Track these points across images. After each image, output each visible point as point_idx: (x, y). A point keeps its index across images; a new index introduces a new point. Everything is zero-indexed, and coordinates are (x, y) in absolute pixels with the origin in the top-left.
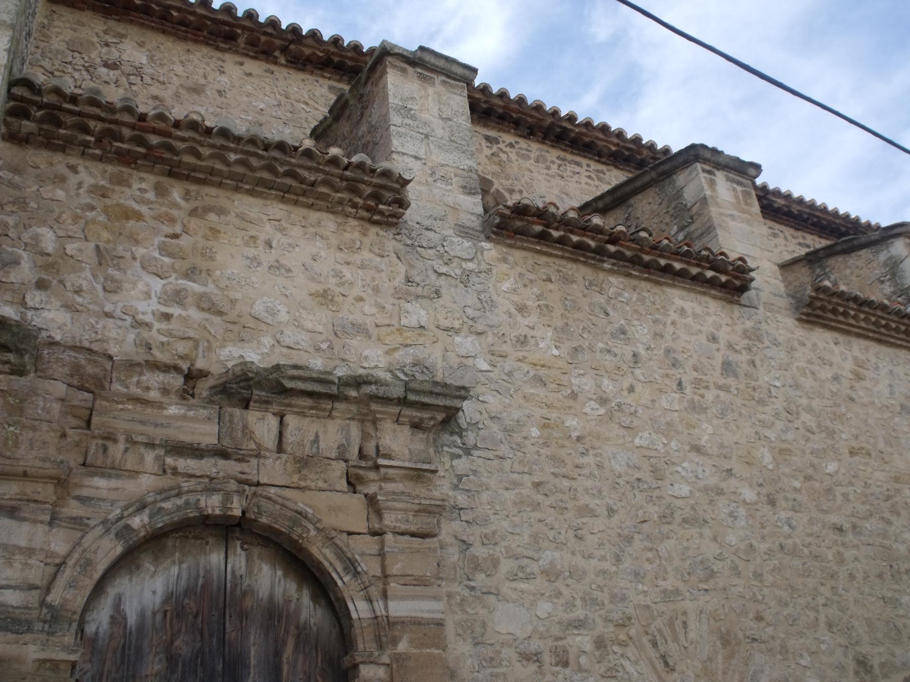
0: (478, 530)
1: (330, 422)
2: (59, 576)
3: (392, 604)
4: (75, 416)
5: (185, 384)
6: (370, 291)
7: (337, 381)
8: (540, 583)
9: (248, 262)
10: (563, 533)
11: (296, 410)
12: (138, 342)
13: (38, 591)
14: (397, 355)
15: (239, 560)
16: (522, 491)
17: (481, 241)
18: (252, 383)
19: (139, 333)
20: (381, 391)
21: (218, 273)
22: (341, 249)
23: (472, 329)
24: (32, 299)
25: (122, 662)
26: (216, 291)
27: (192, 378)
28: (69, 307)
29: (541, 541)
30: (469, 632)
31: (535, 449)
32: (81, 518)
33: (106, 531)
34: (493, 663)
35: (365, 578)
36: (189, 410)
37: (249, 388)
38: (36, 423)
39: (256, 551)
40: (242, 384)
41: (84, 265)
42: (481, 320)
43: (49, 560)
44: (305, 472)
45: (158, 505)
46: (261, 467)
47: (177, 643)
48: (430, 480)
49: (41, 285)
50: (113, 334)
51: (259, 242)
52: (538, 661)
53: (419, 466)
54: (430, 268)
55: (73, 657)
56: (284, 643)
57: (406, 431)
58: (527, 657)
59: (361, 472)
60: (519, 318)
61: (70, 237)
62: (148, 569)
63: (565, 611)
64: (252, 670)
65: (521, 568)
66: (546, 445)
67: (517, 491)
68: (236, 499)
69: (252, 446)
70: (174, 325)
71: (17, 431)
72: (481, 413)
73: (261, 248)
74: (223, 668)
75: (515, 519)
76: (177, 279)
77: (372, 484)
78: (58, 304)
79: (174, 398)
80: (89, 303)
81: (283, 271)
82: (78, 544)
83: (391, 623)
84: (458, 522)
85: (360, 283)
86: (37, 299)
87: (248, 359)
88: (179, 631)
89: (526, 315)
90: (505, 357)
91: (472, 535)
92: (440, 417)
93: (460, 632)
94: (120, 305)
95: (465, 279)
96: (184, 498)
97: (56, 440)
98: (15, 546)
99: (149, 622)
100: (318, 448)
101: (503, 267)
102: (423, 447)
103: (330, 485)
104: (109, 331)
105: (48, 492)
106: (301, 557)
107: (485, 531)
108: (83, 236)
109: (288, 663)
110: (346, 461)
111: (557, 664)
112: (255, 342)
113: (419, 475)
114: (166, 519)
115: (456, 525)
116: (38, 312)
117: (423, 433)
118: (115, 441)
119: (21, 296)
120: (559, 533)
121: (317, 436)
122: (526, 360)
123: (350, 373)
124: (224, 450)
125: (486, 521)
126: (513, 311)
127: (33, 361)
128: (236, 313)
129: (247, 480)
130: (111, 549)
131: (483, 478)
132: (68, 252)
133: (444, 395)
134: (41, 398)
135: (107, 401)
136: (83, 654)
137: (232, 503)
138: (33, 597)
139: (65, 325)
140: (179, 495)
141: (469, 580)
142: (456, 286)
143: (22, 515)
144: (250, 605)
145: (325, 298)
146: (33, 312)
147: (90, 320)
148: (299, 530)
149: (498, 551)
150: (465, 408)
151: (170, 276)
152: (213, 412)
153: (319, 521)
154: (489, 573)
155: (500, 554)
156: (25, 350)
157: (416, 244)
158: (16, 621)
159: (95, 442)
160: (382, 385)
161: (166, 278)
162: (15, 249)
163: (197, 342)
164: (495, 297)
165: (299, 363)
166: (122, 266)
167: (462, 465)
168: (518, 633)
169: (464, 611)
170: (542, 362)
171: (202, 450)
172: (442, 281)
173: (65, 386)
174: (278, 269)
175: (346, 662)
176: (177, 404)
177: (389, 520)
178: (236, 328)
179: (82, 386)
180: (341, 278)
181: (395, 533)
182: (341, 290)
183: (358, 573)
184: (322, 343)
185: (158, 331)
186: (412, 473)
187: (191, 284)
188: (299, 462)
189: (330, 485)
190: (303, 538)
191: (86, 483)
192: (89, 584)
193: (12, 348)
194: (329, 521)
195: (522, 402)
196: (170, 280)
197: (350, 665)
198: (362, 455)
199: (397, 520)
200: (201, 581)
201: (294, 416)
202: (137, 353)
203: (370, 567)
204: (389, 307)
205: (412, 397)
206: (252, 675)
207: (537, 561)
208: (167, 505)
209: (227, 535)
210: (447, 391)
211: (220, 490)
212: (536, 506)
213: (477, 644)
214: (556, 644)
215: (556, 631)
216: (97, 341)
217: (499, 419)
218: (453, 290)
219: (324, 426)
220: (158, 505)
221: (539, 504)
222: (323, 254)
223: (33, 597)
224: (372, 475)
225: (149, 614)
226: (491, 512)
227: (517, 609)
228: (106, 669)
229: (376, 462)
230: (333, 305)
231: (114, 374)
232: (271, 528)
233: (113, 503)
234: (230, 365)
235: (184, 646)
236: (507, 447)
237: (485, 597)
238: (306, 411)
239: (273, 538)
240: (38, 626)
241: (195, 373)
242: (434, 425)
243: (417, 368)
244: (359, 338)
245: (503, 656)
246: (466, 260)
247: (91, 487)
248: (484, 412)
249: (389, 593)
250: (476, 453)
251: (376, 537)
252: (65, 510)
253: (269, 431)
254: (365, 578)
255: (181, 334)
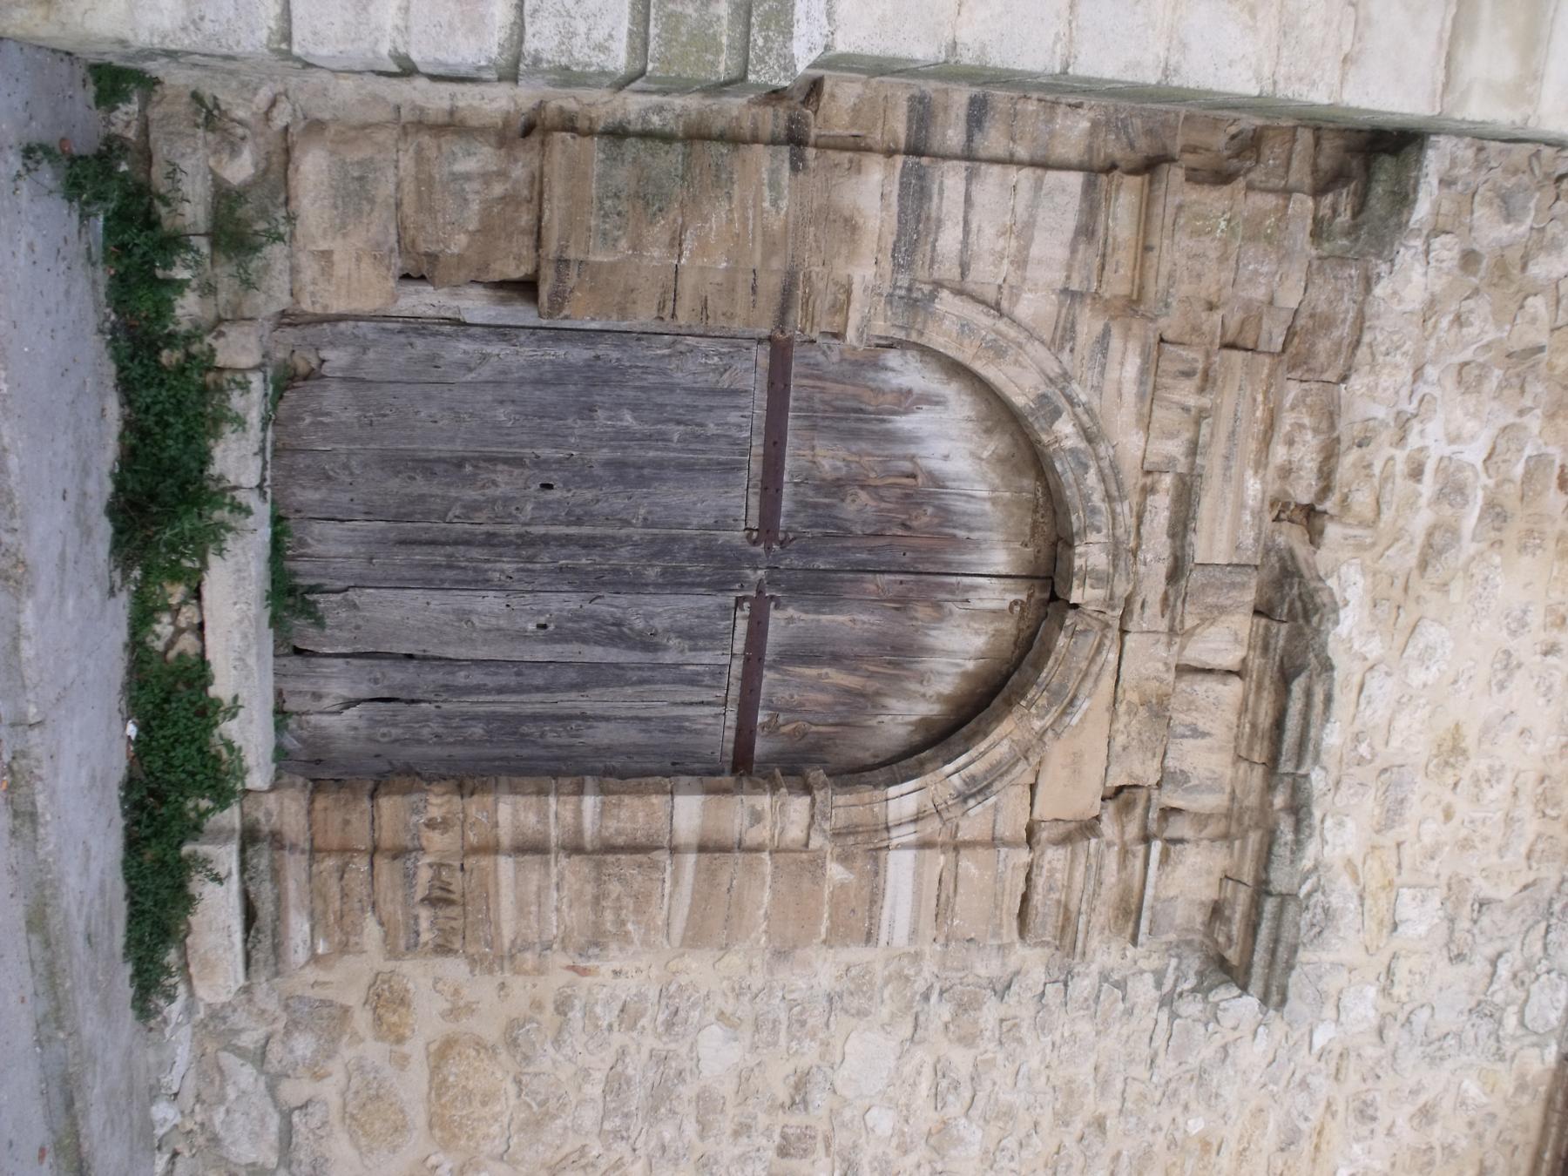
0: (1026, 1013)
1: (1227, 758)
2: (981, 307)
3: (908, 856)
4: (1243, 323)
5: (1297, 505)
6: (1463, 833)
7: (1302, 771)
8: (926, 1117)
9: (1517, 613)
10: (1013, 1165)
11: (1252, 698)
12: (1371, 423)
13: (958, 278)
14: (1345, 880)
15: (995, 597)
16: (1091, 1096)
17: (1559, 1044)
18: (1301, 621)
19: (1387, 425)
20: (1282, 851)
21: (1497, 560)
22: (1542, 781)
23: (1389, 1018)
24: (1444, 246)
25: (837, 410)
26: (1463, 558)
27: (1308, 517)
28: (1432, 306)
29: (1001, 1124)
30: (852, 987)
31: (1166, 1123)
32: (1073, 339)
33: (1051, 380)
34: (796, 1026)
35: (956, 812)
36: (1253, 513)
37: (1292, 616)
38: (1232, 262)
39: (1009, 626)
40: (1298, 604)
41: (1508, 327)
42: (1406, 1036)
43: (1006, 291)
44: (1143, 712)
45: (1092, 463)
46: (1152, 637)
47: (863, 496)
48: (1120, 932)
49: (1469, 259)
50: (1386, 381)
51: (1555, 631)
52: (793, 1103)
53: (1146, 914)
54: (1506, 945)
55: (851, 334)
56: (853, 671)
57: (1209, 894)
58: (801, 1085)
59: (1139, 811)
60: (1409, 1109)
61: (1558, 302)
62: (985, 447)
63: (875, 1158)
64: (811, 617)
65: (956, 1085)
66: (1172, 1143)
67: (1092, 1086)
68: (1100, 593)
69: (1189, 624)
70: (1401, 484)
71: (1218, 233)
72: (1235, 1029)
73: (1543, 636)
74: (819, 570)
75: (1043, 1079)
76: (1485, 487)
77: (1116, 829)
78: (1437, 289)
79: (1274, 488)
80: (1438, 339)
81: (1501, 676)
82: (1031, 335)
83: (876, 854)
84: (1043, 978)
85: (1478, 815)
86: (1445, 254)
87: (1342, 614)
88: (882, 499)
89: (1416, 1121)
90: (1337, 1078)
91: (1020, 1002)
92: (1232, 955)
93: (853, 972)
94: (1437, 392)
95: (1484, 1010)
96: (1103, 506)
97: (1203, 294)
98: (1032, 239)
99: (898, 450)
100: (1183, 736)
101: (1508, 1085)
102: (1178, 921)
103: (1118, 756)
104: (1390, 375)
105: (1118, 284)
106: (997, 701)
107: (1025, 1025)
108: (1559, 323)
109: (820, 676)
110: (1159, 785)
111: (784, 1136)
112: (1371, 627)
113: (1130, 913)
114: (1069, 477)
115: (1037, 975)
116: (1421, 257)
117: (1203, 924)
118: (1201, 390)
119: (1448, 228)
120: (1012, 1158)
121: (1204, 735)
122: (1329, 1117)
123: (1316, 793)
124: (1183, 575)
125: (1041, 1027)
126: (1423, 1099)
127: (1338, 253)
128: (1424, 593)
129: (1131, 612)
130: (1020, 386)
131: (1118, 1026)
132: (1530, 300)
133: (1271, 964)
134: (1274, 268)
135: (1270, 376)
136: (855, 349)
137: (1092, 587)
138: (948, 270)
139: (1400, 301)
140: (1108, 497)
141: (941, 993)
142: (1471, 993)
143: (1081, 247)
144: (919, 615)
145: (1452, 751)
146: (1421, 248)
147: (1409, 343)
148: (1042, 702)
149: (988, 1046)
150: (1246, 999)
151: (1490, 477)
152: (1250, 555)
153: (1058, 736)
154: (952, 1028)
155: (982, 1049)
156: (1357, 239)
157: (1553, 921)
158: (913, 247)
159: (1200, 357)
160: (1293, 852)
161: (1487, 469)
162: (1533, 213)
163: (1372, 524)
164: (1449, 1064)
165: (1335, 706)
166: (1506, 392)
167: (1144, 991)
168: (844, 1072)
169: (887, 983)
170: (1324, 1147)
171: (1184, 536)
172: (1480, 966)
173: (1295, 306)
174: (1506, 667)
175: (816, 774)
176: (1264, 492)
177: (1055, 858)
178: (1397, 592)
179: (1295, 334)
180: (1488, 781)
181: (1031, 866)
182: (1466, 782)
183: (965, 801)
184: (1370, 745)
185: (1391, 458)
186: (1134, 901)
187: (1476, 512)
188: (1160, 703)
189: (1118, 756)
190: (1029, 707)
191: (1130, 346)
192: (965, 356)
193: (1360, 219)
194: (1057, 753)
195: (1253, 1104)
196: (1483, 477)
197: (810, 780)
198: (1168, 812)
199: (1052, 871)
200: (962, 534)
201: (1240, 695)
202: (1352, 423)
203: (975, 819)
204: (1433, 867)
205: (1270, 905)
206: (804, 616)
207: (966, 1115)
208: (1092, 478)
209: (1037, 578)
210: (1279, 970)
211: (1115, 566)
212: (1063, 1119)
213: (830, 1000)
214: (820, 1138)
215: (842, 1139)
216: (1373, 354)
217: (1223, 1061)
218: (1465, 986)
219: (1221, 749)
220: (1092, 463)
221: (1067, 1124)
222: (1533, 748)
223: (948, 270)
224: (1133, 830)
225: (912, 449)
226: (1057, 1038)
227: (885, 1074)
228: (828, 385)
229: (1155, 837)
230: (1437, 766)
231: (1315, 386)
232: (1049, 652)
233: (1098, 389)
234: (1332, 583)
235: (857, 507)
236: (1172, 1074)
237: (910, 1020)
238: (1250, 716)
239: (1030, 655)
240: (904, 280)
241: (1317, 522)
242: (1217, 942)
243: (1320, 916)
244: (1377, 811)
245: (806, 1043)
246: (1522, 1013)
247: (1124, 353)
248: (1237, 1034)
249: (928, 852)
250: (1164, 1016)
251: (1024, 834)
252: (1087, 312)
253: (1217, 651)
254: (956, 812)
255: (1387, 497)
